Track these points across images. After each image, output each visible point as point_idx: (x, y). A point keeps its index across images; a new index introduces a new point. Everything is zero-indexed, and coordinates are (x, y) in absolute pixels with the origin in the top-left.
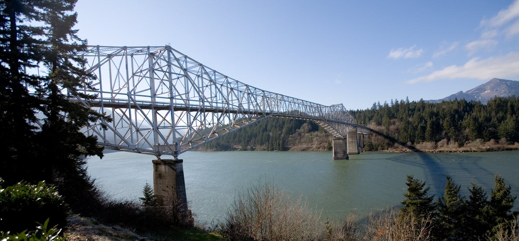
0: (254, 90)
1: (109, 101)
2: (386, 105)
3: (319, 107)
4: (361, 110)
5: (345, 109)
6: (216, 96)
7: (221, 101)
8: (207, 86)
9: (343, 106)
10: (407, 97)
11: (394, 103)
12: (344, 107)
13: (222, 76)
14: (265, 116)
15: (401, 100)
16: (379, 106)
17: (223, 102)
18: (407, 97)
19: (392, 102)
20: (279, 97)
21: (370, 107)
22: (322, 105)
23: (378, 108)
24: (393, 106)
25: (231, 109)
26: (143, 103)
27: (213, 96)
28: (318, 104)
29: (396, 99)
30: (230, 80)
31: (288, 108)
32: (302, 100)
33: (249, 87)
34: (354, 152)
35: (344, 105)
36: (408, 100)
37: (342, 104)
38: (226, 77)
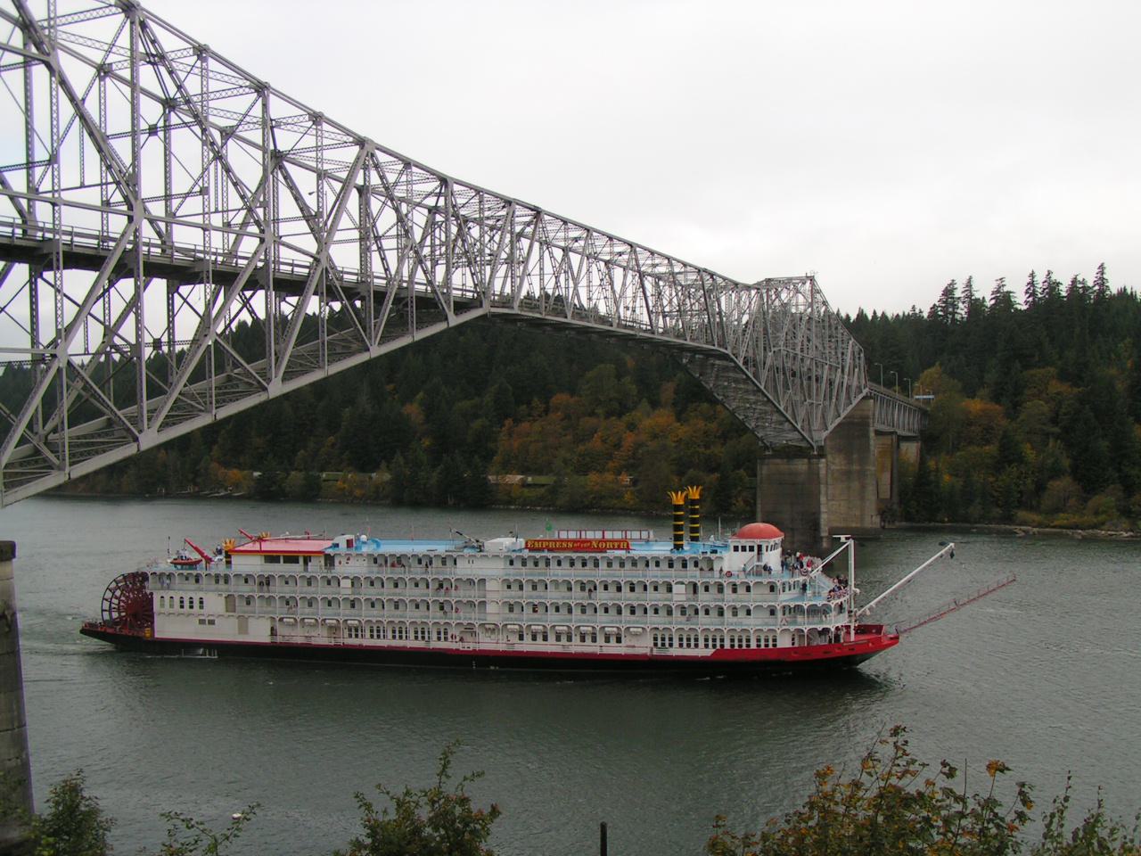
0: (401, 173)
1: (13, 233)
2: (1004, 299)
3: (710, 284)
4: (875, 313)
5: (825, 303)
6: (53, 160)
7: (93, 197)
8: (153, 130)
9: (815, 291)
10: (1102, 267)
11: (1040, 286)
12: (819, 292)
13: (241, 82)
14: (451, 315)
15: (1074, 281)
16: (970, 302)
17: (107, 203)
18: (1102, 267)
19: (1032, 284)
20: (523, 216)
21: (924, 300)
22: (720, 277)
23: (962, 311)
24: (1034, 305)
25: (468, 294)
26: (72, 241)
27: (41, 154)
28: (705, 271)
29: (1049, 273)
30: (278, 109)
31: (674, 294)
32: (631, 245)
33: (378, 153)
34: (854, 525)
35: (821, 283)
36: (1102, 281)
37: (812, 279)
38: (261, 89)
